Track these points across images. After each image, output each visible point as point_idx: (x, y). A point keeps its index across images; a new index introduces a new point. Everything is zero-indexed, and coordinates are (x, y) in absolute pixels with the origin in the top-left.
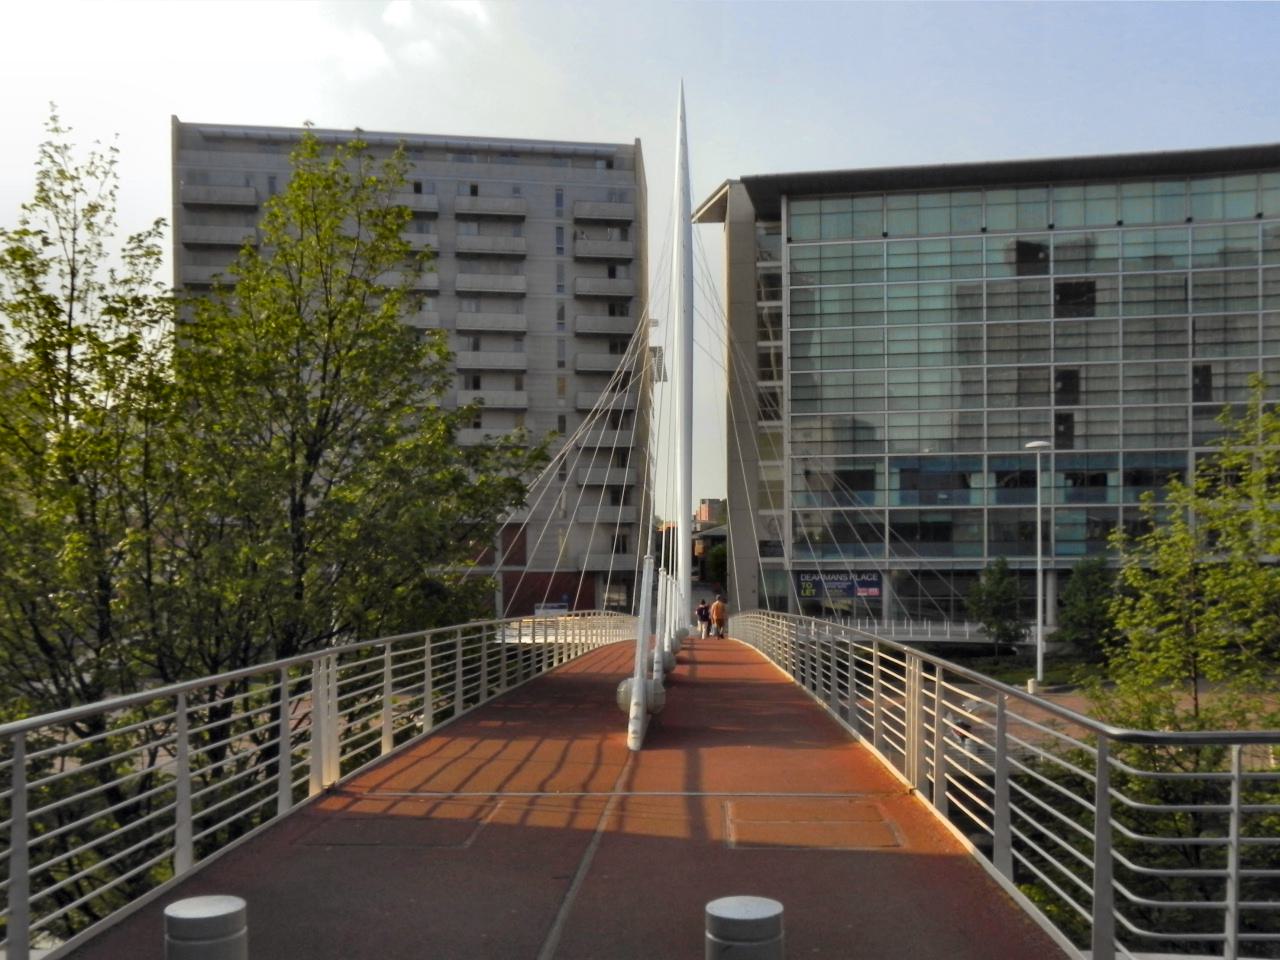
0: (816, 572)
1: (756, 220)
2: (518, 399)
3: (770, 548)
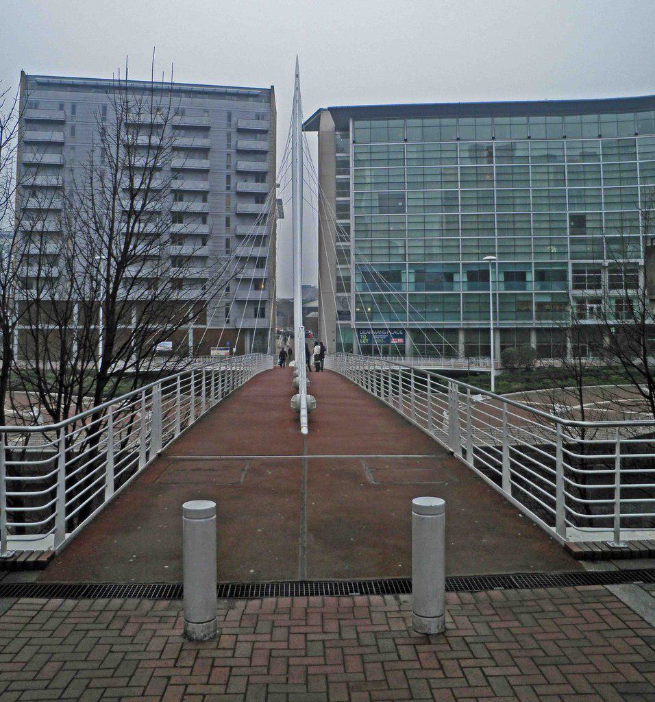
0: (369, 329)
1: (336, 131)
2: (204, 229)
3: (343, 315)
